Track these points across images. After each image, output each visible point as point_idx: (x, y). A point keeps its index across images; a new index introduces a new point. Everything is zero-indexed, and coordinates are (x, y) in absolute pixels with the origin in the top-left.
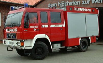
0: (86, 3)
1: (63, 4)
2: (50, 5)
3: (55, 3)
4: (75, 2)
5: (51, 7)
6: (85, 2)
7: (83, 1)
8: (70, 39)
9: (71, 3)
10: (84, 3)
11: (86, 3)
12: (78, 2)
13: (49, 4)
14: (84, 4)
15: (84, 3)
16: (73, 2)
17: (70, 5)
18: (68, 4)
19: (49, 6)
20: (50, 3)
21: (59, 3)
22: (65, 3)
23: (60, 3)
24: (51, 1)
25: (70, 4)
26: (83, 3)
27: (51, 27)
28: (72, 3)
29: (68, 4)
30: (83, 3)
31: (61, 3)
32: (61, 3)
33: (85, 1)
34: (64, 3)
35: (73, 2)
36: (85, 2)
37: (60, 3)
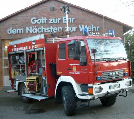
0: (55, 21)
1: (35, 30)
2: (11, 31)
3: (20, 27)
4: (54, 28)
5: (13, 33)
6: (54, 21)
7: (51, 20)
8: (7, 75)
9: (47, 30)
10: (52, 21)
11: (55, 21)
12: (18, 30)
13: (9, 30)
14: (52, 23)
15: (52, 21)
16: (50, 28)
17: (47, 32)
18: (44, 30)
19: (9, 31)
20: (11, 28)
21: (27, 29)
22: (39, 29)
23: (30, 29)
24: (13, 25)
25: (46, 30)
26: (50, 22)
27: (17, 56)
28: (50, 30)
29: (44, 30)
30: (50, 22)
31: (31, 29)
32: (31, 29)
33: (54, 19)
34: (36, 29)
35: (50, 28)
36: (54, 21)
37: (30, 29)
